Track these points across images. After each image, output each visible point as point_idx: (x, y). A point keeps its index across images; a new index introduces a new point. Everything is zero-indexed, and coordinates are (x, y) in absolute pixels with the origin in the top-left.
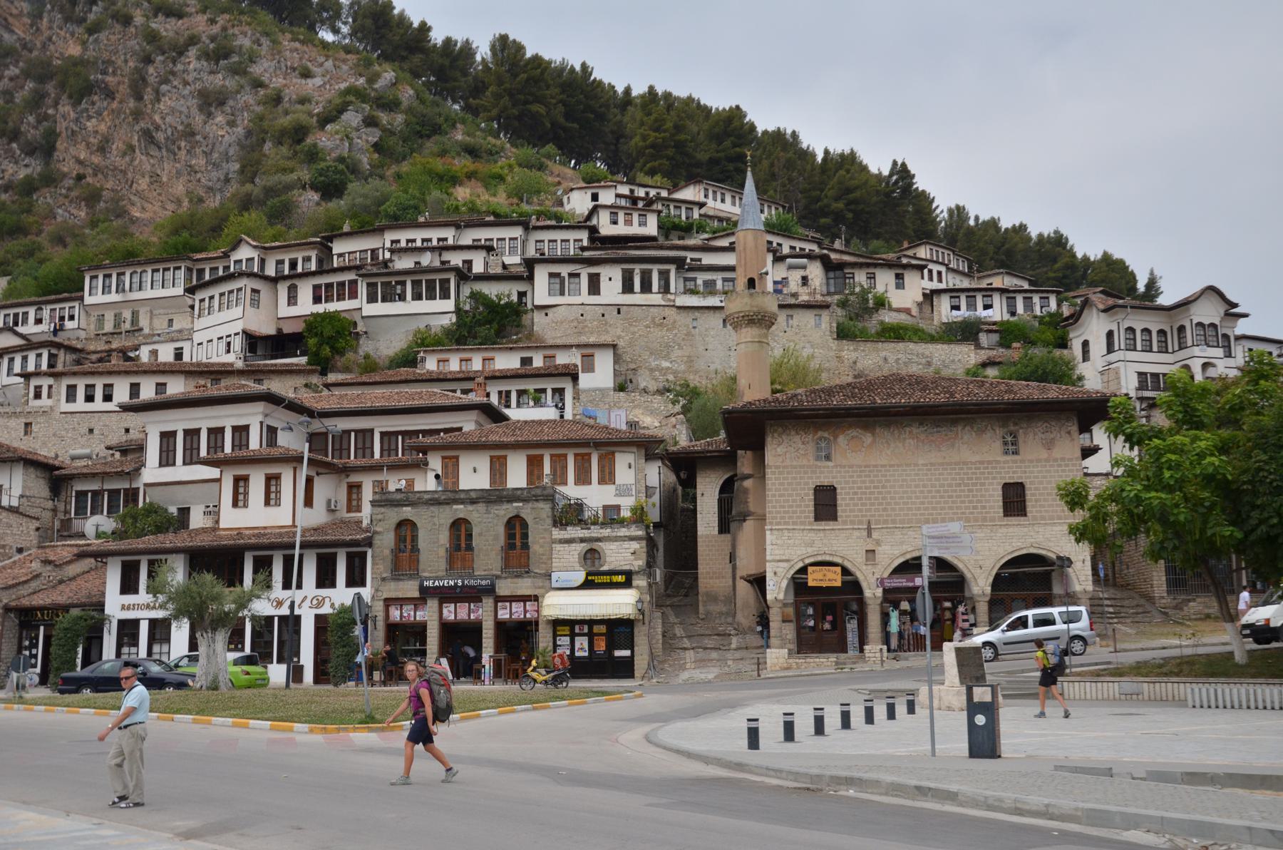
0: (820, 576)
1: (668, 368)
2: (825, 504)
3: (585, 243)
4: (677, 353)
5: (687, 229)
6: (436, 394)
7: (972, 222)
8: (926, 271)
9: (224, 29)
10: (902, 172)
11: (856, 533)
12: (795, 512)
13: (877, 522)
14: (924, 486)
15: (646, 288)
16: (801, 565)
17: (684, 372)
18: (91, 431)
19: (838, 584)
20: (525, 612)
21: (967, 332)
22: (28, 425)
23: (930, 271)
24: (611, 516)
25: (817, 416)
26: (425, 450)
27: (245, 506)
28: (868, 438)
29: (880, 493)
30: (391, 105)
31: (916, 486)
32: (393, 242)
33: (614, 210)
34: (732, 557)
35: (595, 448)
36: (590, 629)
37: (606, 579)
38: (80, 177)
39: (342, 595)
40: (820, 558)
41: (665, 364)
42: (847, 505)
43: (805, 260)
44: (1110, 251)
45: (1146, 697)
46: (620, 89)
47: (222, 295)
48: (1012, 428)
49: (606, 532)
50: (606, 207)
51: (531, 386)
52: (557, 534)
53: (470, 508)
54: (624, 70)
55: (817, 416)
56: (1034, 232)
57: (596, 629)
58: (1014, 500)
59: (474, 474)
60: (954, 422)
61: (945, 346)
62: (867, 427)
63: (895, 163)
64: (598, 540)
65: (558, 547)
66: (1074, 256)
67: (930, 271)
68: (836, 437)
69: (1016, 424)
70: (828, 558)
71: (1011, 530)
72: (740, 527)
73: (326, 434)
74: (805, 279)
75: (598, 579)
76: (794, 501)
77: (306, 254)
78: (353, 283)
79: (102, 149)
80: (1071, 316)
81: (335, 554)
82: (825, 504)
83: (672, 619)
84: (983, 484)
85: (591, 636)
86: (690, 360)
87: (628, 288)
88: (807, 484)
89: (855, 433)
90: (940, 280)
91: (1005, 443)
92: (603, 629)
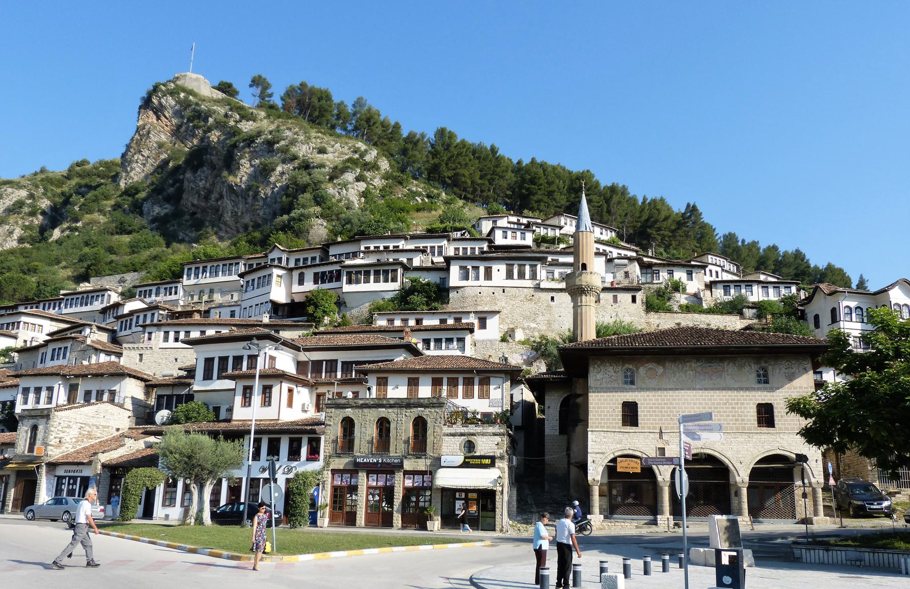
0: (625, 464)
1: (535, 328)
2: (630, 414)
3: (485, 249)
4: (540, 318)
5: (553, 241)
6: (379, 340)
7: (740, 244)
8: (707, 270)
9: (278, 127)
10: (692, 210)
11: (652, 435)
12: (608, 420)
13: (667, 428)
14: (700, 404)
15: (521, 276)
16: (612, 456)
17: (545, 331)
18: (176, 360)
19: (639, 471)
20: (423, 482)
21: (735, 308)
22: (141, 355)
23: (711, 271)
24: (487, 419)
25: (625, 354)
26: (365, 372)
27: (250, 405)
28: (660, 370)
29: (669, 408)
30: (374, 167)
31: (694, 404)
32: (366, 248)
33: (505, 230)
34: (568, 449)
35: (480, 375)
36: (466, 496)
37: (478, 461)
38: (194, 214)
39: (304, 466)
40: (625, 452)
41: (533, 325)
42: (645, 416)
43: (626, 261)
44: (833, 263)
45: (867, 564)
46: (515, 161)
47: (259, 278)
48: (763, 364)
49: (479, 429)
50: (500, 228)
51: (443, 335)
52: (446, 430)
53: (390, 410)
54: (517, 150)
55: (625, 354)
56: (782, 250)
57: (470, 495)
58: (766, 415)
59: (398, 391)
60: (722, 360)
61: (719, 317)
62: (660, 362)
63: (688, 205)
64: (473, 434)
65: (446, 438)
66: (809, 267)
67: (711, 271)
68: (638, 369)
69: (766, 362)
70: (631, 452)
71: (763, 436)
72: (574, 431)
73: (307, 362)
74: (627, 273)
75: (472, 461)
76: (608, 412)
77: (313, 255)
78: (339, 272)
79: (207, 198)
80: (806, 299)
81: (301, 438)
82: (630, 414)
83: (527, 492)
84: (743, 404)
85: (467, 500)
86: (549, 323)
87: (510, 276)
88: (617, 400)
89: (651, 366)
90: (717, 277)
91: (759, 375)
92: (475, 495)
